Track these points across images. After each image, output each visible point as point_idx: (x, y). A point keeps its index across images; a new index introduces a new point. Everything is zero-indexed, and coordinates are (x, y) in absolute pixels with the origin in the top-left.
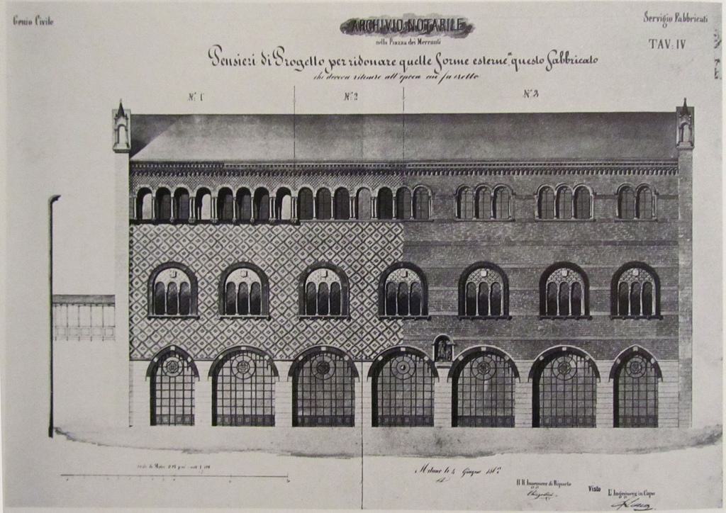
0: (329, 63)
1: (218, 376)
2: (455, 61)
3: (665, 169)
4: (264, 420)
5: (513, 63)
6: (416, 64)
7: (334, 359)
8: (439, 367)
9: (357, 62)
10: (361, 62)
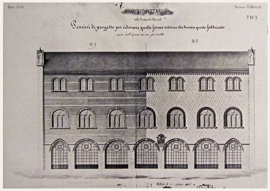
0: (97, 28)
1: (167, 150)
2: (173, 27)
3: (240, 73)
4: (144, 167)
5: (141, 28)
6: (170, 28)
7: (90, 143)
8: (160, 146)
9: (126, 28)
10: (127, 27)
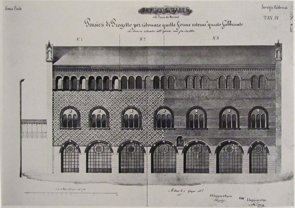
0: (134, 26)
1: (88, 152)
2: (185, 25)
3: (270, 68)
4: (107, 170)
5: (208, 26)
6: (169, 26)
7: (136, 146)
8: (178, 149)
9: (145, 25)
10: (147, 25)
